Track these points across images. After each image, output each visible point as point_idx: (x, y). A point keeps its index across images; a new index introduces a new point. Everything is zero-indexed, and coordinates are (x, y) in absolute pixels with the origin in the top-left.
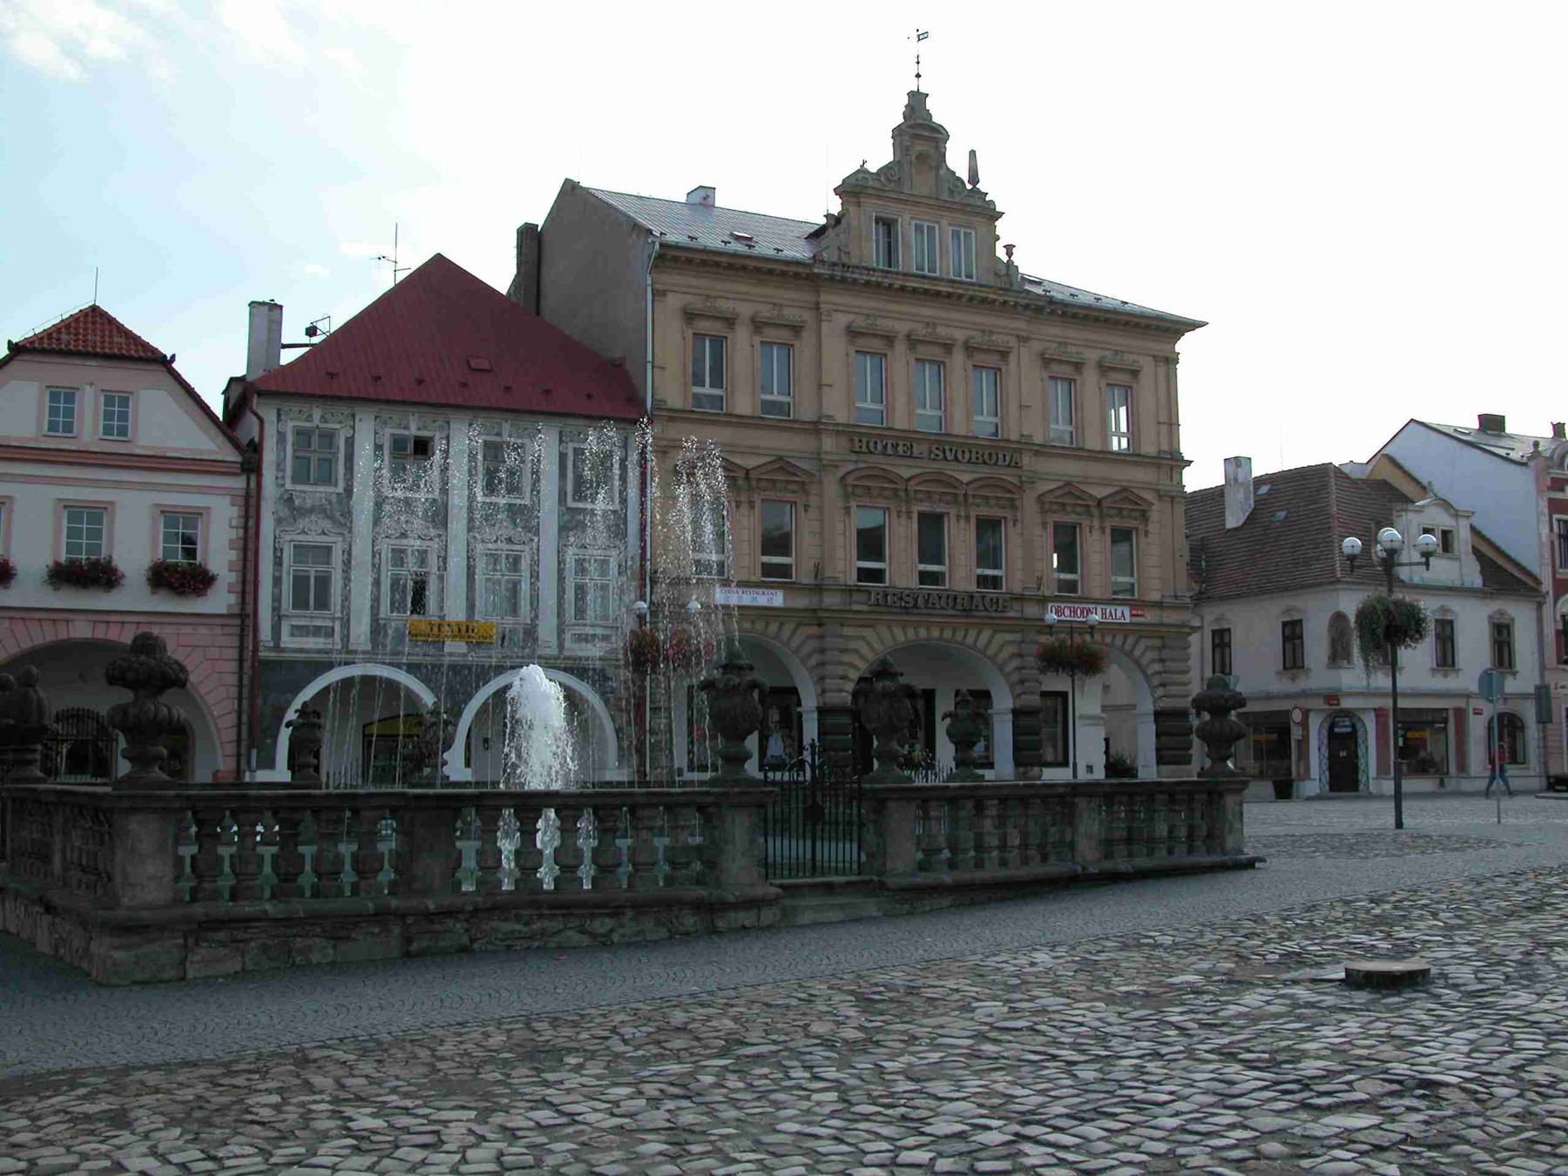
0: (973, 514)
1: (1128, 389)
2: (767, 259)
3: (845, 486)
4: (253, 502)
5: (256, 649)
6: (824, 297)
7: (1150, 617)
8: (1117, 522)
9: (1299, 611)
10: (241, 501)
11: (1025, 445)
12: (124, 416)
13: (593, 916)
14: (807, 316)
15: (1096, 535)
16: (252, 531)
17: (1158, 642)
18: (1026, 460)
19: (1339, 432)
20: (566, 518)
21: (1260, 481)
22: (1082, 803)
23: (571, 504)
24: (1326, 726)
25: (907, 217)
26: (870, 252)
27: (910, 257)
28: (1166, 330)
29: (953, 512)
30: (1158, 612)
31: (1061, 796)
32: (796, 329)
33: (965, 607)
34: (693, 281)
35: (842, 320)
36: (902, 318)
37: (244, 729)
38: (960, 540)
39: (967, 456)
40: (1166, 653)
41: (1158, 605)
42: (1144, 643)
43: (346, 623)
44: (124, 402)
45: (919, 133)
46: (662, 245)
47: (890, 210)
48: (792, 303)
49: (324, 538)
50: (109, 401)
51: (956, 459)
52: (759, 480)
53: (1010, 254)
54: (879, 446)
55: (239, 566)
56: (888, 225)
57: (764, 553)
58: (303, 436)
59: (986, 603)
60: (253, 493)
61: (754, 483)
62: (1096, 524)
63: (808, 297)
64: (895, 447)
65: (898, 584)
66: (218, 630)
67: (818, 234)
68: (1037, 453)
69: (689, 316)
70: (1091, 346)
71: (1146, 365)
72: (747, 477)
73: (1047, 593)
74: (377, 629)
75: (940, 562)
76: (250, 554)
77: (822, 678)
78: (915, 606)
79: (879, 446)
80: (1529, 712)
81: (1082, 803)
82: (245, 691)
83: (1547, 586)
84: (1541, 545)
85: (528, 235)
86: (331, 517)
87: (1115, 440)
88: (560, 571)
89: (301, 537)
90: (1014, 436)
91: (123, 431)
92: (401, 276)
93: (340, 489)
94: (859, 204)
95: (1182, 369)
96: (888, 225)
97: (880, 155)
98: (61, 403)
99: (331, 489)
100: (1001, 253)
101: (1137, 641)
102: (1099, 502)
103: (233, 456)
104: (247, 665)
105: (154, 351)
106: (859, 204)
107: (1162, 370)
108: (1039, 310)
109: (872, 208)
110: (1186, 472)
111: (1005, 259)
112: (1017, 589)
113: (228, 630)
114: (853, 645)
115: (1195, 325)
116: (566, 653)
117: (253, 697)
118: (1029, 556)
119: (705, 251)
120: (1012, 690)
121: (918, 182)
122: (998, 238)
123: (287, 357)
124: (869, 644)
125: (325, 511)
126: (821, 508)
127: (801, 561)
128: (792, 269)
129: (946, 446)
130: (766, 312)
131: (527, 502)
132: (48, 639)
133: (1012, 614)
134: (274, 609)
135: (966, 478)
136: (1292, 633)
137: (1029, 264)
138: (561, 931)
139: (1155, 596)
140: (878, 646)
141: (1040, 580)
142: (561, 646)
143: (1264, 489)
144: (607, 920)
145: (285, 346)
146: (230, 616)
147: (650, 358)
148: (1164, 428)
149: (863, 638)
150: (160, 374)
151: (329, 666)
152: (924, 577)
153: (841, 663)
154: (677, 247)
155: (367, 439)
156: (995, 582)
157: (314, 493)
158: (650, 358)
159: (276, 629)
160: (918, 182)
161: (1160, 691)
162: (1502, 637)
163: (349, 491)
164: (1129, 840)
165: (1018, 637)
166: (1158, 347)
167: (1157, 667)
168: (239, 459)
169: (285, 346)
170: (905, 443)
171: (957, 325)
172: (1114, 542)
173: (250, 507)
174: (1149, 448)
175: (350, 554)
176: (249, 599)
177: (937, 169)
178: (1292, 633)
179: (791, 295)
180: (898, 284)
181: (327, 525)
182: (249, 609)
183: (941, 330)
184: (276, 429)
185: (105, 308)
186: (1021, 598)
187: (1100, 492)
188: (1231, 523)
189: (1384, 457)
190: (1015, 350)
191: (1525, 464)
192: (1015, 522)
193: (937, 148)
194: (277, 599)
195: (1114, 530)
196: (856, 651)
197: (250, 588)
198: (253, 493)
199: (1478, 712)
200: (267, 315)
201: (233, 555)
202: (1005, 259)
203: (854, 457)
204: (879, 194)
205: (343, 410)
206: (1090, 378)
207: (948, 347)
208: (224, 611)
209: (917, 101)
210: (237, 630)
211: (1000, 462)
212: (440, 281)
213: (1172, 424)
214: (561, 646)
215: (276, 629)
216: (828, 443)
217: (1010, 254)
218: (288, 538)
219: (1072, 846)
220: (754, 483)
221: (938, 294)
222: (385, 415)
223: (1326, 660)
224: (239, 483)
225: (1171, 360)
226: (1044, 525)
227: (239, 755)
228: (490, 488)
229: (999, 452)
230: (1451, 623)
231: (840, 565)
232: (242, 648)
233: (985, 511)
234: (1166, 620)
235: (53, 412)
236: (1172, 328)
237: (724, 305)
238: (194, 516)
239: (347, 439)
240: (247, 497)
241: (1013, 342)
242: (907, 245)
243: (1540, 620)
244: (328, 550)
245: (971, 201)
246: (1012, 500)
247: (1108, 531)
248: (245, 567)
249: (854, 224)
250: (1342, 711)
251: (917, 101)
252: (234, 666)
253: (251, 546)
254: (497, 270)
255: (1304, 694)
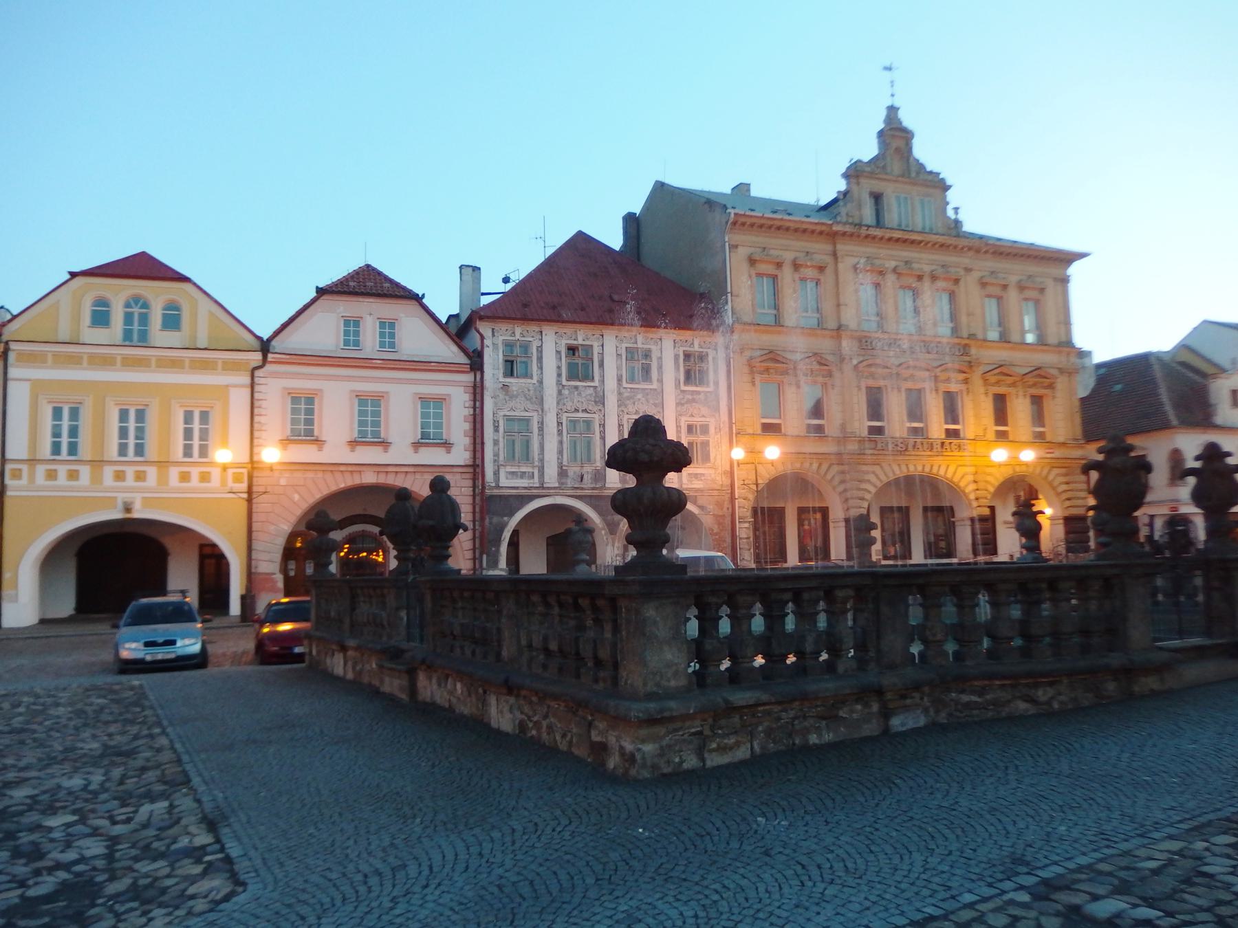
4: (478, 390)
5: (484, 487)
9: (1144, 449)
10: (471, 390)
12: (392, 335)
13: (1036, 685)
19: (1158, 335)
21: (1099, 366)
32: (821, 269)
34: (754, 238)
43: (542, 470)
44: (392, 325)
45: (895, 136)
47: (878, 186)
49: (527, 414)
50: (382, 325)
53: (956, 213)
55: (471, 433)
56: (877, 198)
58: (509, 345)
60: (478, 384)
70: (1015, 272)
71: (1050, 284)
74: (562, 473)
77: (846, 500)
91: (392, 345)
92: (550, 251)
93: (534, 381)
94: (858, 184)
96: (877, 198)
97: (868, 150)
98: (352, 326)
100: (950, 213)
103: (463, 359)
104: (478, 498)
105: (410, 291)
106: (858, 184)
109: (868, 185)
111: (953, 217)
114: (866, 477)
115: (1082, 256)
117: (482, 519)
122: (948, 203)
123: (485, 301)
124: (877, 476)
127: (832, 423)
138: (1009, 701)
140: (898, 472)
143: (1102, 371)
144: (1048, 689)
145: (483, 294)
149: (874, 473)
150: (412, 306)
151: (532, 498)
153: (859, 489)
155: (550, 343)
159: (497, 473)
163: (541, 382)
166: (1054, 271)
167: (1064, 487)
168: (467, 361)
169: (483, 294)
171: (925, 261)
173: (477, 392)
176: (479, 455)
184: (494, 342)
185: (375, 265)
189: (1184, 347)
194: (496, 455)
196: (869, 481)
198: (478, 384)
200: (471, 273)
204: (871, 175)
205: (534, 328)
206: (1013, 296)
209: (892, 110)
212: (581, 247)
215: (497, 473)
217: (956, 213)
221: (913, 242)
222: (561, 331)
224: (468, 378)
225: (1065, 281)
227: (474, 559)
231: (857, 424)
232: (474, 487)
235: (346, 333)
236: (1065, 259)
240: (475, 387)
241: (962, 272)
251: (892, 110)
253: (478, 419)
254: (614, 239)
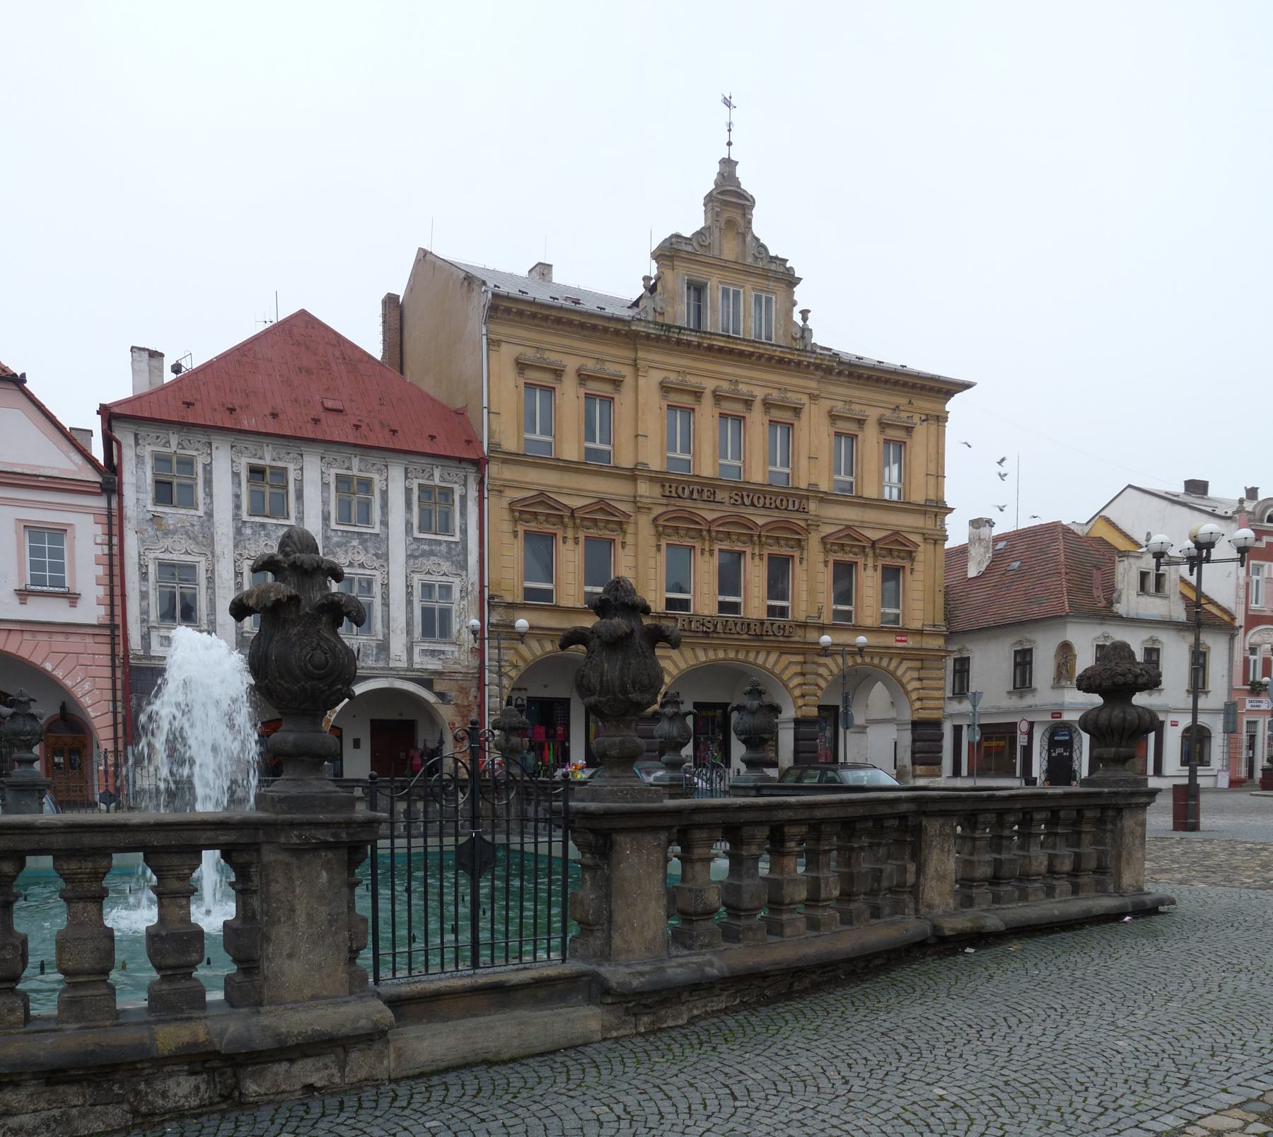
0: (766, 552)
1: (901, 445)
2: (591, 315)
3: (656, 526)
6: (641, 354)
7: (911, 642)
8: (888, 561)
10: (105, 520)
11: (813, 493)
14: (626, 371)
15: (870, 571)
16: (116, 550)
17: (918, 664)
18: (813, 506)
19: (1064, 497)
20: (414, 546)
22: (933, 827)
23: (417, 534)
24: (1047, 735)
25: (714, 279)
26: (680, 313)
27: (714, 320)
28: (939, 391)
29: (748, 550)
30: (918, 638)
31: (903, 817)
33: (758, 635)
35: (656, 376)
36: (713, 377)
37: (120, 728)
38: (755, 575)
39: (762, 501)
40: (923, 674)
41: (920, 632)
42: (906, 664)
46: (495, 295)
47: (700, 273)
48: (613, 359)
51: (753, 504)
52: (583, 519)
53: (805, 319)
54: (687, 492)
55: (107, 580)
56: (698, 289)
57: (586, 584)
59: (777, 631)
60: (115, 512)
61: (578, 521)
62: (870, 563)
63: (630, 354)
64: (701, 492)
65: (700, 612)
66: (89, 640)
67: (636, 304)
68: (822, 500)
69: (522, 366)
72: (572, 516)
73: (826, 622)
75: (737, 594)
76: (116, 570)
78: (714, 631)
79: (687, 492)
80: (1216, 725)
81: (933, 827)
82: (119, 694)
83: (1240, 620)
84: (1238, 586)
85: (391, 302)
86: (194, 539)
87: (887, 489)
88: (409, 594)
89: (167, 556)
90: (803, 485)
93: (201, 512)
95: (950, 426)
96: (698, 289)
97: (691, 221)
99: (192, 512)
100: (797, 318)
101: (901, 663)
102: (874, 543)
107: (933, 428)
108: (829, 371)
110: (948, 518)
111: (801, 323)
112: (801, 617)
113: (98, 639)
116: (416, 666)
118: (811, 588)
119: (533, 303)
120: (795, 703)
121: (723, 251)
122: (794, 304)
125: (187, 532)
126: (636, 545)
128: (612, 326)
129: (744, 492)
130: (590, 365)
131: (377, 530)
132: (33, 659)
133: (796, 639)
134: (143, 621)
135: (760, 521)
136: (1023, 661)
137: (822, 336)
139: (917, 625)
141: (820, 610)
142: (410, 658)
143: (1001, 545)
146: (100, 626)
147: (485, 404)
148: (932, 480)
152: (723, 607)
154: (507, 298)
156: (783, 611)
157: (173, 515)
158: (485, 404)
159: (146, 638)
160: (723, 251)
161: (918, 705)
162: (1199, 661)
163: (210, 515)
164: (995, 880)
165: (800, 658)
167: (916, 684)
168: (100, 480)
170: (708, 489)
171: (758, 383)
172: (884, 580)
173: (114, 523)
174: (918, 497)
175: (213, 571)
176: (118, 611)
177: (744, 236)
178: (1023, 661)
179: (613, 351)
180: (706, 343)
181: (193, 547)
182: (118, 621)
183: (743, 388)
186: (804, 626)
187: (874, 535)
188: (972, 573)
189: (1101, 518)
190: (807, 406)
191: (1229, 518)
192: (801, 559)
193: (744, 215)
194: (145, 612)
195: (885, 568)
197: (118, 600)
198: (115, 512)
199: (1175, 724)
201: (101, 571)
202: (801, 323)
203: (665, 501)
204: (692, 258)
207: (748, 403)
208: (95, 622)
209: (728, 165)
210: (108, 640)
211: (790, 507)
212: (301, 336)
213: (939, 476)
214: (410, 658)
215: (146, 638)
216: (643, 488)
217: (805, 319)
218: (152, 556)
219: (915, 891)
220: (578, 521)
222: (241, 445)
223: (1051, 682)
224: (100, 503)
226: (826, 563)
228: (344, 518)
229: (788, 499)
230: (1158, 650)
232: (113, 655)
233: (776, 550)
234: (925, 646)
236: (945, 389)
237: (552, 357)
238: (59, 533)
239: (205, 466)
240: (110, 515)
241: (805, 399)
242: (714, 310)
243: (1231, 649)
244: (192, 568)
245: (773, 267)
246: (799, 540)
247: (879, 568)
248: (111, 581)
249: (670, 285)
250: (1063, 722)
252: (108, 672)
255: (1030, 709)
